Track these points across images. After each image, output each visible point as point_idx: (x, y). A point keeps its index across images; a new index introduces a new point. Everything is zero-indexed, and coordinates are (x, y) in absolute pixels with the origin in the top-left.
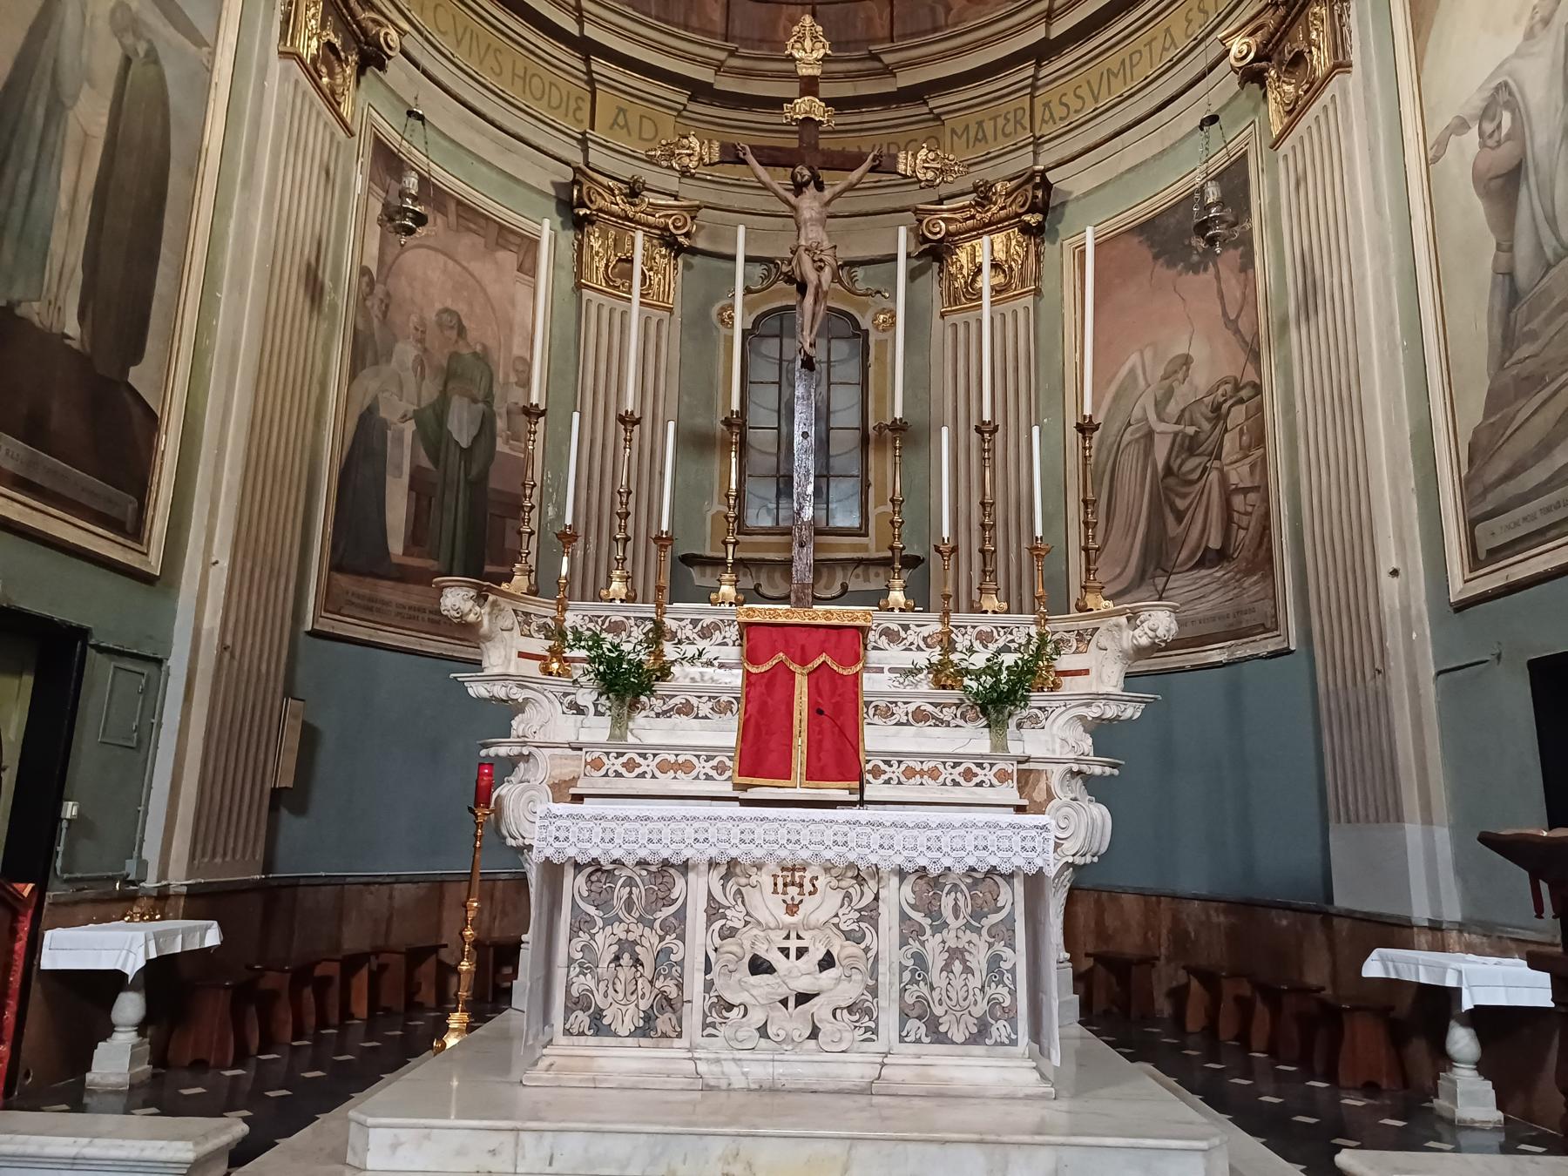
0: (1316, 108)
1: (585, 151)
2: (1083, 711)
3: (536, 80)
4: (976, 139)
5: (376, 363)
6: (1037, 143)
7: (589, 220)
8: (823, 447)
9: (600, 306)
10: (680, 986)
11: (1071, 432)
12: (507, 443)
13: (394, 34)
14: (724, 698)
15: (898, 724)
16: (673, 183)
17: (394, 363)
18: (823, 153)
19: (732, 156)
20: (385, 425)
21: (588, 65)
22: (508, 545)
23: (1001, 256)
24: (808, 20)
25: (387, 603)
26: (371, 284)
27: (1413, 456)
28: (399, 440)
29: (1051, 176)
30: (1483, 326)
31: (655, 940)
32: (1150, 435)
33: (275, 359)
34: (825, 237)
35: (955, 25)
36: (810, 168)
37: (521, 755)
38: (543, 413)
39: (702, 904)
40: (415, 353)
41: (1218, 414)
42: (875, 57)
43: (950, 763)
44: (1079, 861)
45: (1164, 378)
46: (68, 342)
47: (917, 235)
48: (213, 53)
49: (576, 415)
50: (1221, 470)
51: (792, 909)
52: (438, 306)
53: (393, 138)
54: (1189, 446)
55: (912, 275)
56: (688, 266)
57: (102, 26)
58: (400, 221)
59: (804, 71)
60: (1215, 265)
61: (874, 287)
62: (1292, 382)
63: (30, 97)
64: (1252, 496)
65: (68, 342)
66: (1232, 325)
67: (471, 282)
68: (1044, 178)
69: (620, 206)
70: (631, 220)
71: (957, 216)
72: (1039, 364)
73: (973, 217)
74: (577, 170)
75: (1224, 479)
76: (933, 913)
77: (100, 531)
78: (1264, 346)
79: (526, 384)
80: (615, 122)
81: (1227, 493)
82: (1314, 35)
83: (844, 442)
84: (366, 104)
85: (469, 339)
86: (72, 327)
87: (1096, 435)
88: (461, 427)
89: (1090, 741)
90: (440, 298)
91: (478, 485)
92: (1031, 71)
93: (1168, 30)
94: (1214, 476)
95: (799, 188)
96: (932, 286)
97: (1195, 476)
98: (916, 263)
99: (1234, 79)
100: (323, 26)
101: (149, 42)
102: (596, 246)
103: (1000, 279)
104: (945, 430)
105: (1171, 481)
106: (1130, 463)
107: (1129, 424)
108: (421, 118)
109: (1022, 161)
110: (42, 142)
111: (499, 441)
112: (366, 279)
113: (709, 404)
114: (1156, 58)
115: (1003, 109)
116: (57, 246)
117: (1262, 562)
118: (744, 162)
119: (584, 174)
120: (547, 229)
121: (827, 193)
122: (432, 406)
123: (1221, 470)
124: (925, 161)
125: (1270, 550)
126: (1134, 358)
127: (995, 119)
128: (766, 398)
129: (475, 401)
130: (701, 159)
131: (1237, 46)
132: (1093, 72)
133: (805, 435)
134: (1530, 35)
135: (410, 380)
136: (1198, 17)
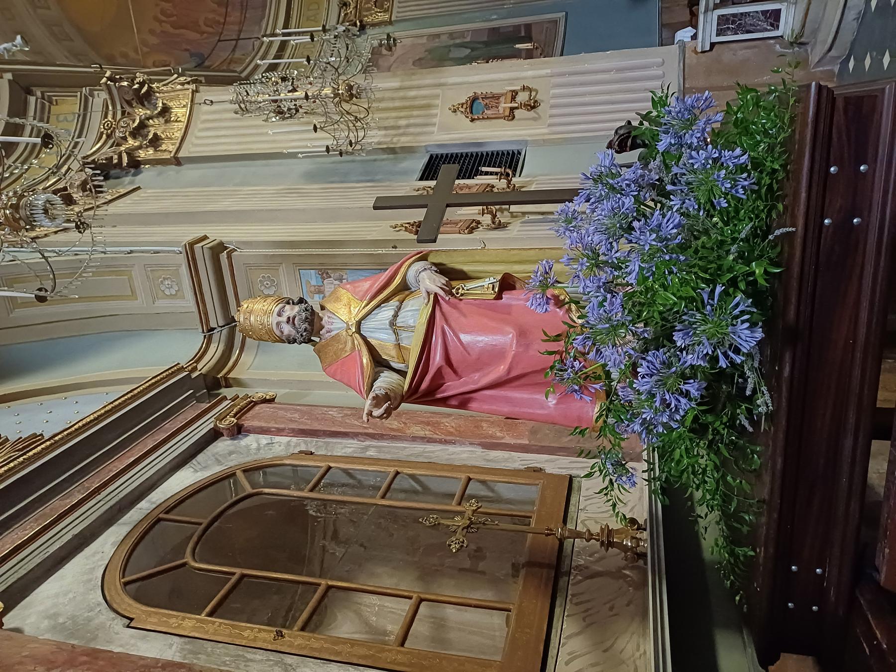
9: (398, 12)
79: (438, 36)
91: (486, 44)
111: (466, 40)
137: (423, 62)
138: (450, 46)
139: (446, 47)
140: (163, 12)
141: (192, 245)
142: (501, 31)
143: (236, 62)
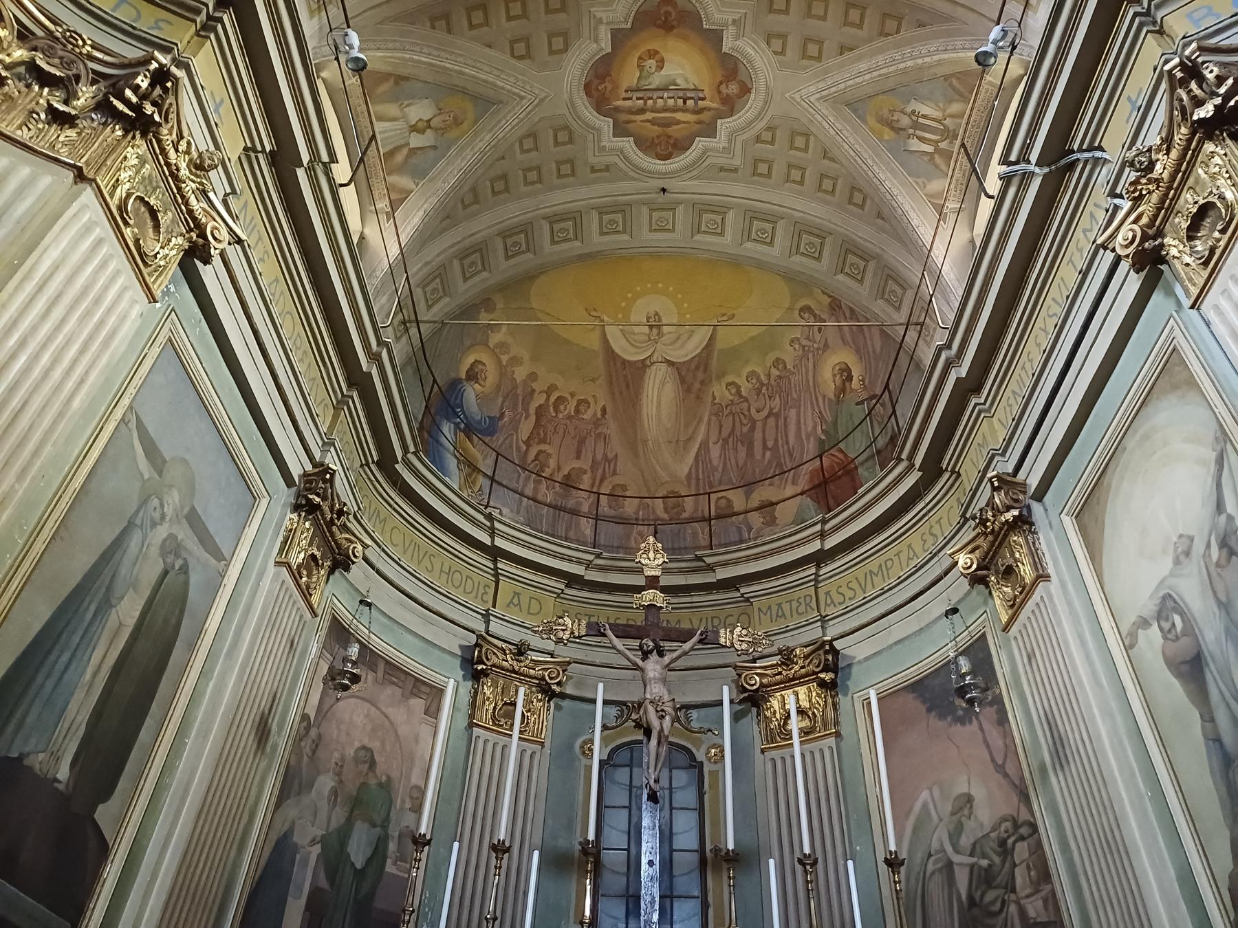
0: (1030, 604)
1: (487, 623)
6: (823, 620)
7: (484, 673)
8: (667, 866)
9: (486, 741)
11: (883, 867)
12: (395, 864)
13: (359, 547)
16: (550, 645)
18: (663, 629)
19: (596, 630)
20: (295, 849)
21: (495, 565)
23: (805, 704)
24: (651, 539)
27: (1183, 896)
28: (305, 863)
29: (837, 645)
30: (1209, 782)
32: (949, 865)
33: (218, 793)
34: (666, 692)
35: (755, 539)
36: (653, 641)
38: (429, 843)
40: (333, 784)
41: (1005, 850)
42: (699, 559)
45: (953, 814)
46: (56, 785)
47: (737, 686)
48: (228, 566)
49: (456, 845)
50: (1017, 902)
52: (357, 744)
53: (346, 617)
54: (983, 878)
55: (736, 717)
57: (154, 551)
58: (339, 680)
60: (977, 719)
61: (706, 726)
62: (1058, 816)
63: (88, 599)
65: (56, 785)
66: (1000, 769)
67: (387, 723)
68: (832, 646)
69: (509, 662)
70: (516, 673)
71: (768, 672)
72: (842, 800)
73: (780, 673)
74: (479, 636)
75: (1022, 912)
78: (1031, 789)
79: (418, 810)
80: (511, 602)
82: (1017, 555)
83: (685, 862)
84: (333, 594)
85: (378, 772)
86: (63, 773)
87: (903, 869)
88: (358, 852)
90: (361, 738)
92: (813, 570)
93: (910, 546)
94: (1013, 908)
95: (646, 655)
96: (752, 726)
98: (739, 708)
99: (965, 583)
100: (310, 544)
101: (185, 559)
102: (488, 693)
103: (806, 723)
104: (772, 862)
105: (976, 911)
106: (936, 890)
107: (930, 855)
108: (369, 605)
109: (814, 633)
110: (87, 630)
111: (389, 861)
112: (305, 724)
113: (570, 826)
114: (904, 564)
115: (796, 596)
118: (604, 635)
119: (484, 639)
120: (454, 687)
121: (667, 659)
122: (339, 830)
123: (1017, 902)
124: (740, 636)
126: (925, 795)
128: (618, 820)
129: (374, 825)
130: (572, 633)
131: (963, 559)
132: (860, 572)
133: (651, 863)
134: (1177, 562)
135: (324, 806)
136: (931, 540)
139: (387, 819)
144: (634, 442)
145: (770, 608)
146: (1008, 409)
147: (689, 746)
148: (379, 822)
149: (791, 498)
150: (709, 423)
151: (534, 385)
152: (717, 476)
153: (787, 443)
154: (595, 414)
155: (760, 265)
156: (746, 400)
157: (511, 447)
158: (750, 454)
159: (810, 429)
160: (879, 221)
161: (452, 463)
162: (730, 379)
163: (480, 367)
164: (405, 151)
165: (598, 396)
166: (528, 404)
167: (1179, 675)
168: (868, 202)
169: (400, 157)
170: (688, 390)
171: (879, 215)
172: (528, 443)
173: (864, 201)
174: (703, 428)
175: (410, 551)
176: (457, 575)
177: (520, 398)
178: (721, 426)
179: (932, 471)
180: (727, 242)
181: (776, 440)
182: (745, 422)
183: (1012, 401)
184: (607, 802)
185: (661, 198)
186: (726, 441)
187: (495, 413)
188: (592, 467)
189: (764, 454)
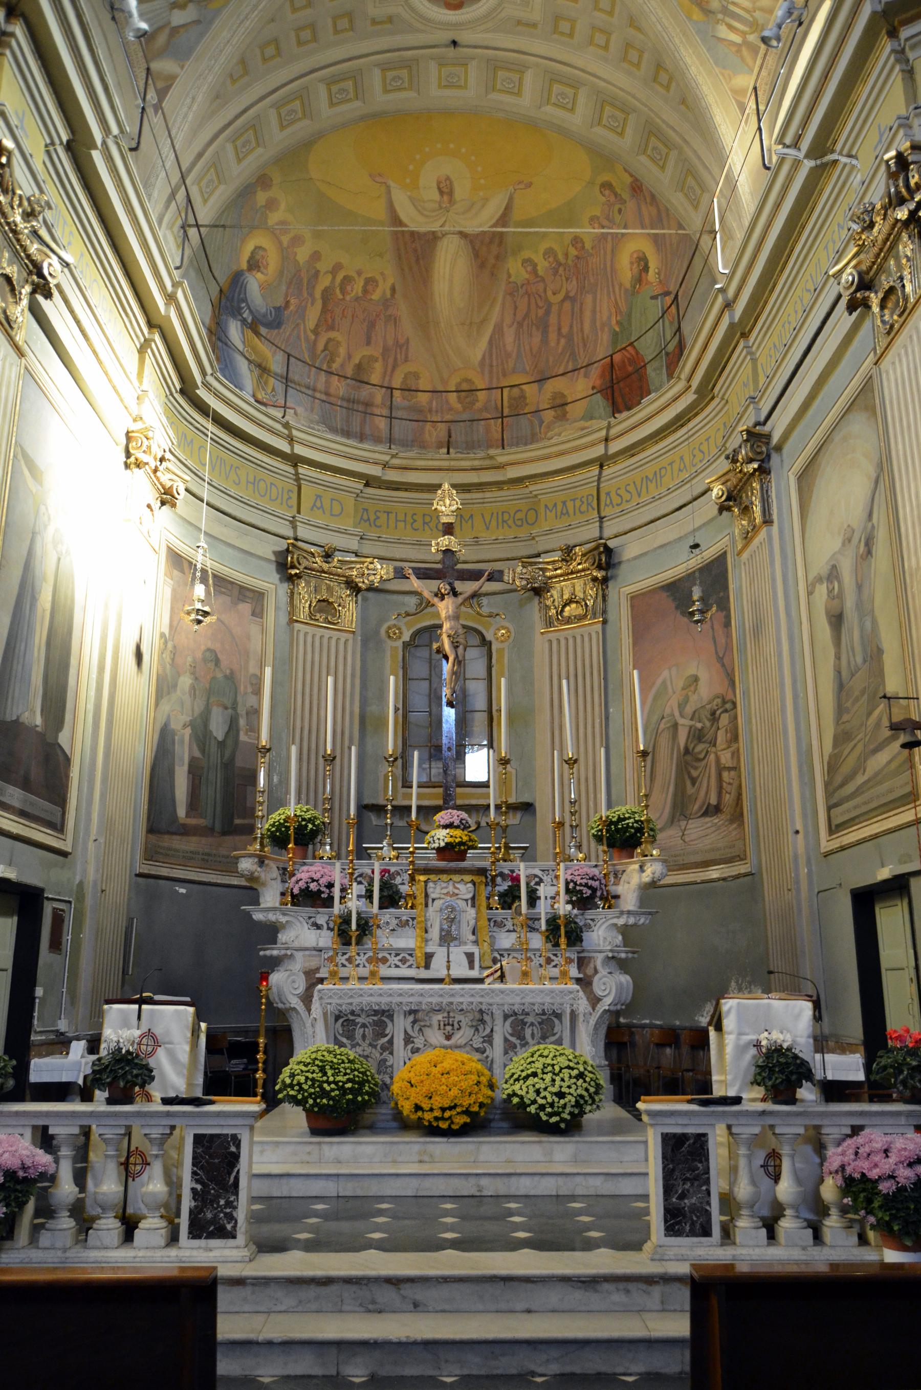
1: (295, 528)
2: (615, 921)
3: (262, 483)
4: (562, 513)
5: (169, 693)
7: (298, 576)
9: (306, 634)
10: (391, 1078)
12: (246, 734)
14: (404, 918)
15: (508, 931)
17: (178, 692)
20: (174, 733)
22: (248, 805)
25: (176, 850)
26: (166, 643)
28: (182, 742)
31: (378, 1055)
32: (675, 726)
37: (286, 955)
39: (402, 1036)
41: (714, 717)
42: (491, 458)
43: (538, 954)
44: (612, 1008)
45: (683, 689)
51: (448, 1038)
54: (698, 736)
56: (365, 600)
59: (445, 520)
61: (495, 611)
64: (732, 773)
66: (720, 659)
76: (521, 1037)
77: (49, 831)
79: (258, 692)
80: (314, 505)
81: (720, 769)
86: (39, 721)
89: (620, 938)
91: (228, 766)
97: (702, 756)
105: (688, 758)
107: (663, 718)
111: (242, 734)
114: (675, 475)
116: (33, 678)
117: (738, 817)
125: (742, 808)
126: (665, 674)
127: (574, 500)
129: (226, 708)
134: (843, 544)
137: (211, 665)
138: (234, 708)
140: (347, 280)
141: (260, 247)
142: (249, 788)
143: (260, 376)
144: (426, 323)
145: (555, 505)
146: (831, 244)
147: (480, 628)
148: (229, 706)
149: (580, 387)
150: (503, 304)
151: (319, 266)
152: (511, 364)
153: (582, 331)
154: (384, 292)
155: (563, 132)
156: (543, 280)
157: (299, 337)
158: (545, 341)
159: (605, 319)
160: (683, 107)
161: (243, 366)
162: (526, 254)
163: (261, 253)
164: (167, 31)
165: (386, 272)
166: (314, 287)
167: (830, 623)
168: (674, 84)
169: (162, 39)
170: (482, 266)
171: (684, 101)
172: (316, 332)
173: (669, 83)
174: (497, 309)
175: (217, 468)
176: (262, 483)
177: (305, 281)
178: (516, 308)
179: (706, 393)
180: (526, 101)
181: (571, 327)
182: (541, 304)
183: (836, 237)
184: (411, 674)
185: (451, 52)
186: (520, 325)
187: (280, 302)
188: (383, 354)
189: (558, 340)
